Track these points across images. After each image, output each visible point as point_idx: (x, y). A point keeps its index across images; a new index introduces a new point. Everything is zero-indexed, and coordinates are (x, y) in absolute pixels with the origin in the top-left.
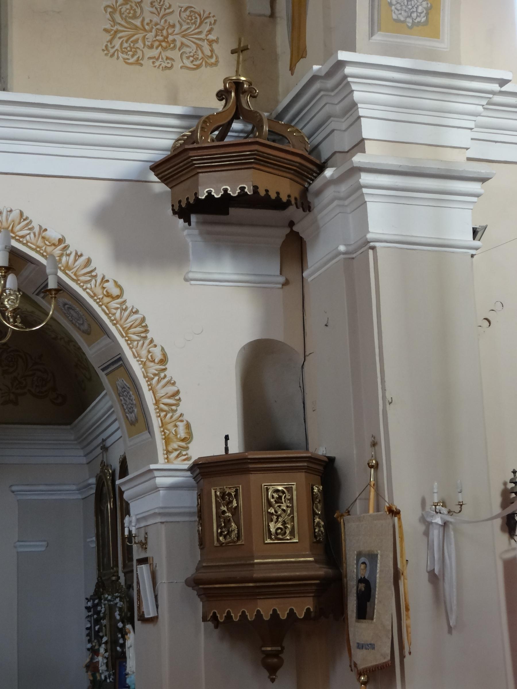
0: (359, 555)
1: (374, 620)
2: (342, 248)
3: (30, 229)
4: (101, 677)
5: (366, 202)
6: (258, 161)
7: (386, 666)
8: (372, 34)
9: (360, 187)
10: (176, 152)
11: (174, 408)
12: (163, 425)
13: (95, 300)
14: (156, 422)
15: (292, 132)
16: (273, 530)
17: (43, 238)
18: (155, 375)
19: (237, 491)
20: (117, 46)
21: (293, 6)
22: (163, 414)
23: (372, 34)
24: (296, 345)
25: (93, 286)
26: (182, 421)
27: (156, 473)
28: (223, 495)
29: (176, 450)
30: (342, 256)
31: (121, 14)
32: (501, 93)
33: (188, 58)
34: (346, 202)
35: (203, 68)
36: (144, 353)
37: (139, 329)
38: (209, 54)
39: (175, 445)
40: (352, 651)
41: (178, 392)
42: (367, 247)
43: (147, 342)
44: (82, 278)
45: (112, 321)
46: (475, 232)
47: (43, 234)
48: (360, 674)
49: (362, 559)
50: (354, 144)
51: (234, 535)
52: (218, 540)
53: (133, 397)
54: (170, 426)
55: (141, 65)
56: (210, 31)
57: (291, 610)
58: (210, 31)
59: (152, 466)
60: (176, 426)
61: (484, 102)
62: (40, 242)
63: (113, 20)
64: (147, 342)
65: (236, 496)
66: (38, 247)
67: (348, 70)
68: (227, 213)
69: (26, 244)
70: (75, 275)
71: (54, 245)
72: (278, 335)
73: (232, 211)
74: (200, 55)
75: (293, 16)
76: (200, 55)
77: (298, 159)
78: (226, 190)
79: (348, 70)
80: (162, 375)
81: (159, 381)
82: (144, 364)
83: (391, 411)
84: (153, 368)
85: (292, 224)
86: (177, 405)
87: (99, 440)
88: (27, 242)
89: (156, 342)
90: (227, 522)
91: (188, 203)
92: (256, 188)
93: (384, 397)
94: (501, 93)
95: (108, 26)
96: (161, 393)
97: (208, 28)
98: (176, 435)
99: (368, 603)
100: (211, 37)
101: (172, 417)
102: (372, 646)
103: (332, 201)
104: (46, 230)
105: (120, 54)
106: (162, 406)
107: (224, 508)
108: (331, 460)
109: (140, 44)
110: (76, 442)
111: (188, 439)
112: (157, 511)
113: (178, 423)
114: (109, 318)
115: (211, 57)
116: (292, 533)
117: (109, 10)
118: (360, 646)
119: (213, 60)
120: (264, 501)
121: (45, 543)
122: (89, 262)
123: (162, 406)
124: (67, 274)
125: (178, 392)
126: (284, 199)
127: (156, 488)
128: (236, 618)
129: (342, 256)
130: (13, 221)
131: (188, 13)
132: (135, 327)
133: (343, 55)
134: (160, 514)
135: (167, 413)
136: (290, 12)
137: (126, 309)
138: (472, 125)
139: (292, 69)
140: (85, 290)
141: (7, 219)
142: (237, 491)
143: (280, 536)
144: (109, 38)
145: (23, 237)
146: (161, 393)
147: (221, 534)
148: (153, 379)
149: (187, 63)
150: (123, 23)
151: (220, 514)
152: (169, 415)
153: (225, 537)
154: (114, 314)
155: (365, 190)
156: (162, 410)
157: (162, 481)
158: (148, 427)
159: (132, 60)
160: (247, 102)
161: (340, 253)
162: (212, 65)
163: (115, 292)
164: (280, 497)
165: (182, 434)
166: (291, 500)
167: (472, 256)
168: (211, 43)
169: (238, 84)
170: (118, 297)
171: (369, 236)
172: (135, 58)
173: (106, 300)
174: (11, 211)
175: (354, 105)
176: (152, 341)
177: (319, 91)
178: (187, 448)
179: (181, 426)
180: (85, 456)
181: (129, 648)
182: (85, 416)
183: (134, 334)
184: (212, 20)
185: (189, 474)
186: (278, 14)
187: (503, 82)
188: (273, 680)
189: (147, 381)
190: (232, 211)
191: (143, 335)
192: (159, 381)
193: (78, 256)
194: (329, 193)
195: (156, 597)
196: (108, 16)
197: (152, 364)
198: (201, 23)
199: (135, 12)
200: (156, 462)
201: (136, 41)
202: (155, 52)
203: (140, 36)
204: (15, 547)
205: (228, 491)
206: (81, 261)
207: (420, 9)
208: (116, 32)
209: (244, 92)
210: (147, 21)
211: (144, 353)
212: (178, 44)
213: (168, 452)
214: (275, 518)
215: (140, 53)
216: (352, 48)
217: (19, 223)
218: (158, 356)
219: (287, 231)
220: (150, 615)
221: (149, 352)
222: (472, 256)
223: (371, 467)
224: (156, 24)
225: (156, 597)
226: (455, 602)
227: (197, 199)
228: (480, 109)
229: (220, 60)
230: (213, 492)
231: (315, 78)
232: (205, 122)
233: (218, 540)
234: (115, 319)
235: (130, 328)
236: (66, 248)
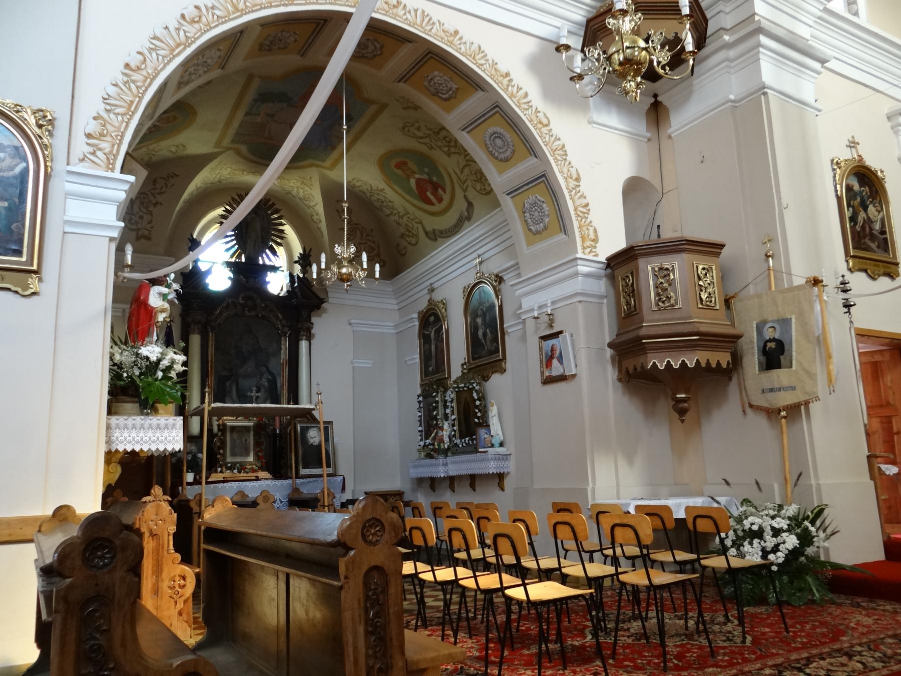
1: (794, 368)
2: (732, 97)
3: (486, 60)
4: (444, 446)
5: (759, 59)
7: (791, 407)
11: (586, 215)
13: (532, 124)
17: (495, 69)
18: (573, 188)
22: (580, 219)
24: (656, 183)
25: (530, 114)
26: (591, 226)
27: (579, 262)
29: (589, 247)
30: (730, 104)
34: (733, 64)
36: (565, 170)
37: (560, 152)
42: (762, 92)
43: (567, 163)
44: (523, 106)
45: (544, 142)
46: (816, 101)
47: (496, 66)
50: (741, 20)
54: (584, 228)
60: (588, 229)
62: (493, 72)
64: (567, 163)
65: (673, 270)
66: (492, 75)
69: (484, 71)
70: (518, 102)
71: (502, 76)
72: (646, 176)
80: (578, 189)
81: (576, 194)
84: (572, 183)
87: (428, 283)
88: (485, 70)
89: (573, 164)
93: (780, 203)
98: (588, 236)
99: (781, 357)
101: (585, 222)
104: (496, 64)
106: (578, 212)
110: (392, 293)
111: (596, 240)
112: (579, 291)
113: (589, 228)
114: (542, 140)
121: (372, 362)
122: (526, 95)
123: (578, 212)
124: (512, 100)
127: (577, 274)
130: (474, 51)
132: (559, 150)
137: (552, 136)
140: (525, 115)
141: (470, 49)
143: (708, 303)
145: (482, 65)
146: (578, 202)
148: (572, 191)
152: (584, 220)
154: (545, 138)
155: (761, 49)
156: (578, 216)
157: (583, 269)
163: (545, 121)
165: (592, 236)
167: (817, 115)
170: (547, 125)
173: (539, 126)
174: (472, 43)
176: (570, 163)
178: (595, 247)
179: (591, 229)
180: (397, 304)
181: (492, 417)
182: (416, 267)
183: (558, 155)
189: (569, 192)
191: (564, 157)
192: (576, 194)
193: (519, 89)
197: (571, 180)
204: (352, 363)
206: (521, 93)
211: (565, 170)
213: (584, 248)
217: (479, 54)
218: (575, 176)
219: (653, 100)
220: (572, 372)
221: (569, 171)
222: (817, 115)
230: (650, 268)
234: (545, 142)
235: (555, 150)
236: (511, 81)
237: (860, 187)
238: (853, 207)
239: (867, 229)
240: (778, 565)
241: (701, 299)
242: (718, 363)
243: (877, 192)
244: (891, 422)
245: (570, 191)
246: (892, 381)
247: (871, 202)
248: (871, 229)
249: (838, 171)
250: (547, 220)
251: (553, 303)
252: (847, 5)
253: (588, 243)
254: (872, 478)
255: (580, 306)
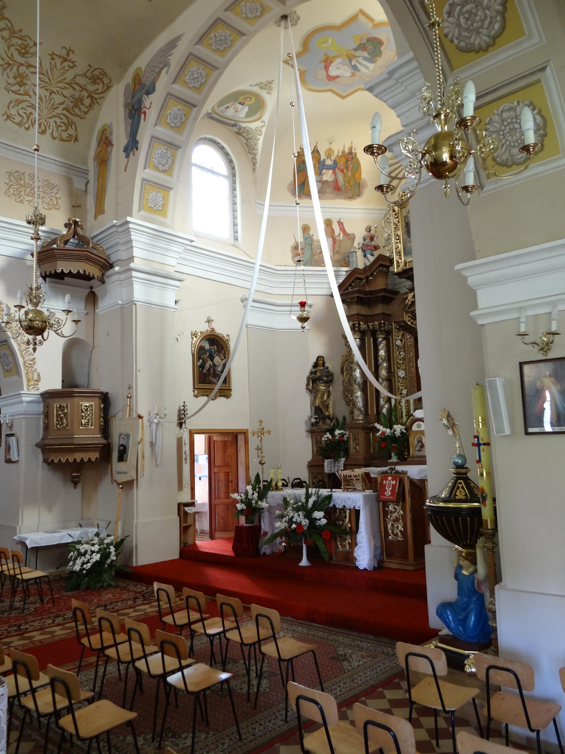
0: (120, 435)
2: (120, 302)
6: (87, 259)
8: (139, 211)
9: (132, 277)
10: (43, 250)
12: (27, 373)
14: (23, 372)
15: (99, 248)
16: (83, 423)
18: (24, 350)
19: (67, 405)
20: (11, 192)
21: (97, 190)
22: (27, 368)
23: (139, 211)
24: (90, 341)
27: (23, 395)
28: (60, 406)
31: (14, 177)
32: (191, 246)
33: (46, 204)
34: (123, 282)
35: (52, 210)
38: (56, 203)
39: (32, 383)
40: (114, 475)
41: (34, 359)
46: (176, 302)
48: (119, 485)
49: (122, 437)
51: (65, 425)
52: (56, 426)
53: (10, 359)
54: (30, 374)
55: (23, 203)
56: (56, 193)
57: (89, 458)
58: (56, 193)
59: (21, 392)
60: (33, 374)
61: (183, 248)
63: (10, 179)
65: (67, 407)
67: (131, 225)
68: (63, 279)
72: (81, 335)
73: (66, 278)
74: (52, 204)
75: (97, 193)
76: (52, 204)
77: (103, 261)
78: (70, 270)
79: (131, 225)
80: (28, 350)
81: (26, 353)
82: (19, 345)
83: (139, 374)
85: (91, 288)
86: (34, 365)
90: (62, 418)
91: (50, 273)
92: (85, 271)
94: (191, 246)
95: (7, 182)
96: (27, 358)
97: (56, 191)
98: (33, 378)
100: (57, 196)
102: (126, 473)
103: (117, 281)
105: (13, 196)
107: (60, 413)
108: (107, 393)
109: (23, 193)
111: (38, 380)
115: (57, 205)
116: (92, 425)
117: (8, 174)
118: (118, 473)
119: (57, 207)
120: (80, 410)
123: (27, 365)
125: (34, 359)
126: (91, 276)
127: (22, 402)
128: (56, 461)
129: (119, 306)
131: (46, 182)
133: (129, 219)
134: (24, 414)
135: (29, 368)
136: (96, 192)
138: (177, 257)
139: (95, 218)
142: (67, 405)
144: (7, 187)
146: (27, 358)
147: (58, 424)
149: (45, 206)
150: (15, 181)
151: (58, 415)
152: (30, 369)
153: (60, 425)
155: (133, 279)
156: (27, 366)
157: (25, 399)
158: (19, 373)
159: (18, 200)
160: (79, 231)
161: (119, 304)
162: (57, 209)
164: (87, 409)
166: (92, 410)
168: (57, 198)
169: (76, 222)
171: (134, 299)
172: (20, 199)
175: (131, 241)
177: (113, 232)
178: (38, 385)
179: (35, 374)
184: (58, 188)
185: (40, 396)
186: (88, 191)
187: (192, 241)
188: (75, 488)
190: (66, 278)
192: (26, 353)
194: (115, 278)
195: (18, 451)
196: (7, 177)
198: (53, 188)
199: (21, 177)
200: (23, 390)
201: (21, 191)
202: (30, 198)
203: (23, 189)
205: (63, 405)
207: (160, 204)
208: (11, 185)
209: (79, 226)
210: (26, 182)
212: (41, 197)
213: (29, 386)
214: (84, 418)
215: (22, 198)
216: (131, 216)
219: (89, 290)
223: (128, 397)
224: (31, 185)
225: (18, 451)
226: (160, 454)
227: (56, 272)
228: (181, 251)
229: (61, 207)
230: (55, 405)
231: (114, 226)
232: (61, 237)
233: (56, 426)
237: (210, 346)
238: (203, 359)
239: (212, 371)
240: (87, 570)
241: (82, 424)
242: (82, 459)
243: (222, 348)
244: (228, 475)
245: (21, 352)
246: (231, 453)
247: (217, 355)
248: (214, 370)
249: (195, 339)
250: (11, 365)
251: (10, 416)
252: (232, 225)
253: (32, 383)
254: (179, 515)
255: (24, 420)
